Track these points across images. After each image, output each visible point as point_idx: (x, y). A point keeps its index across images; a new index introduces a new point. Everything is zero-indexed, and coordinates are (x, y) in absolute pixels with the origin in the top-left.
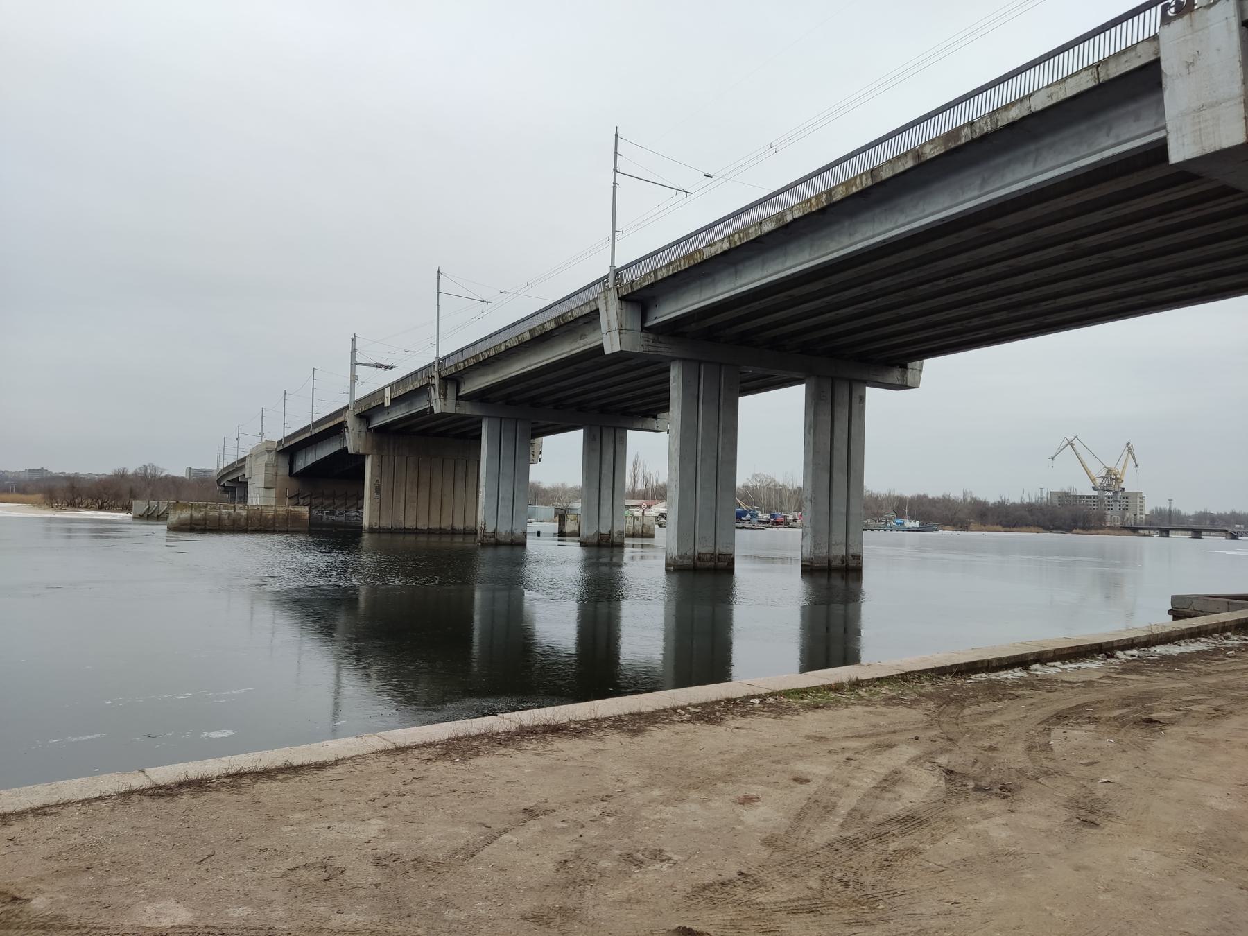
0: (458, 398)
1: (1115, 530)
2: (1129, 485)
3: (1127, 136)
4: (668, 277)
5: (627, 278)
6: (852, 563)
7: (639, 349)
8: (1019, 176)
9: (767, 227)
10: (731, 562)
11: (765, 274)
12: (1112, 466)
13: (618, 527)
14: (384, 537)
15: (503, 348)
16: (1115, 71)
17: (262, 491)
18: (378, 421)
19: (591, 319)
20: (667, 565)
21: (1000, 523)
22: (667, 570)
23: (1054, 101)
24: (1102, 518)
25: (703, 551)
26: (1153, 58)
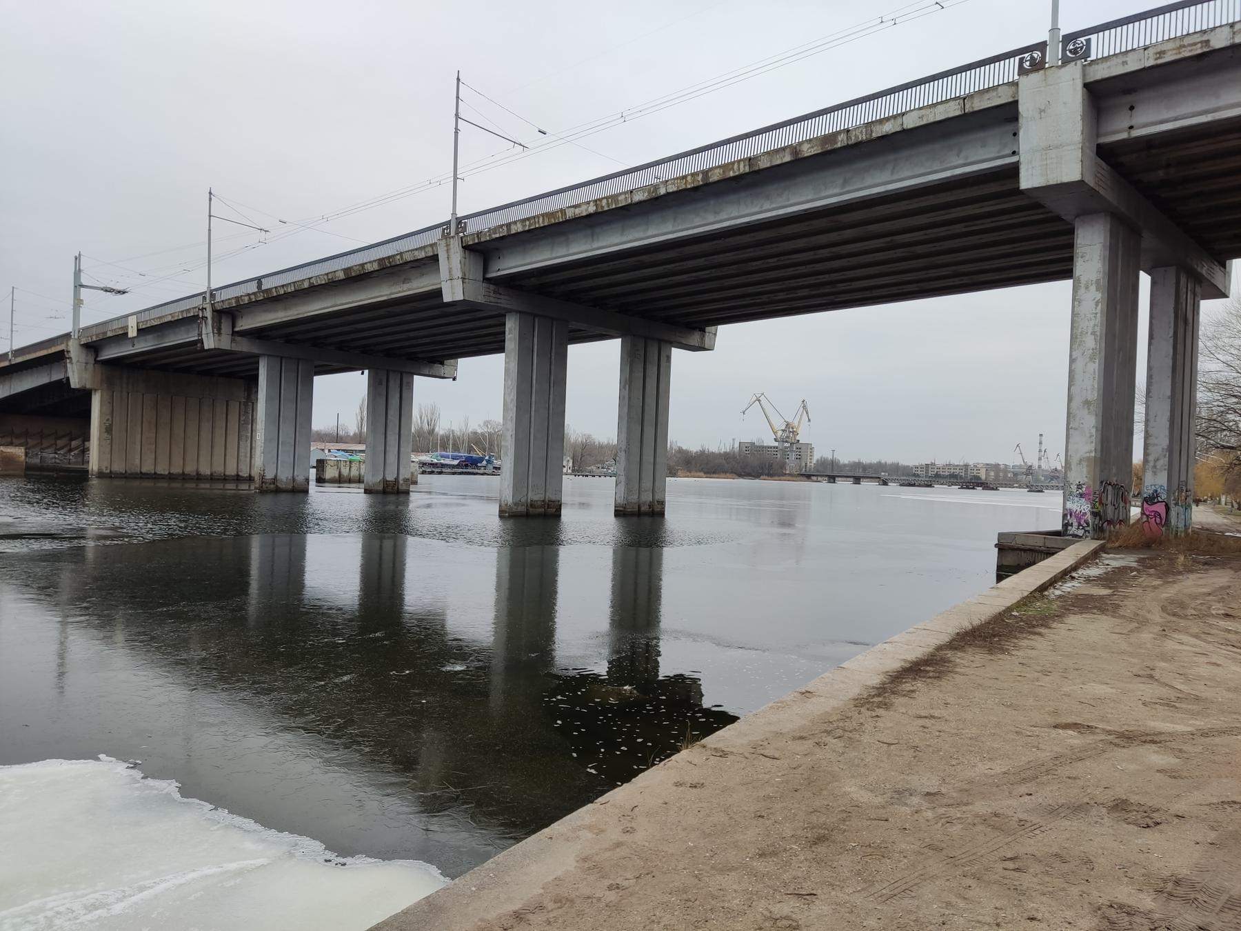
0: (234, 333)
2: (803, 438)
5: (472, 227)
6: (657, 508)
7: (481, 299)
9: (638, 197)
11: (625, 239)
13: (404, 474)
14: (117, 482)
15: (306, 285)
16: (979, 104)
18: (110, 353)
19: (430, 262)
20: (501, 511)
21: (701, 471)
22: (501, 517)
23: (924, 122)
24: (783, 466)
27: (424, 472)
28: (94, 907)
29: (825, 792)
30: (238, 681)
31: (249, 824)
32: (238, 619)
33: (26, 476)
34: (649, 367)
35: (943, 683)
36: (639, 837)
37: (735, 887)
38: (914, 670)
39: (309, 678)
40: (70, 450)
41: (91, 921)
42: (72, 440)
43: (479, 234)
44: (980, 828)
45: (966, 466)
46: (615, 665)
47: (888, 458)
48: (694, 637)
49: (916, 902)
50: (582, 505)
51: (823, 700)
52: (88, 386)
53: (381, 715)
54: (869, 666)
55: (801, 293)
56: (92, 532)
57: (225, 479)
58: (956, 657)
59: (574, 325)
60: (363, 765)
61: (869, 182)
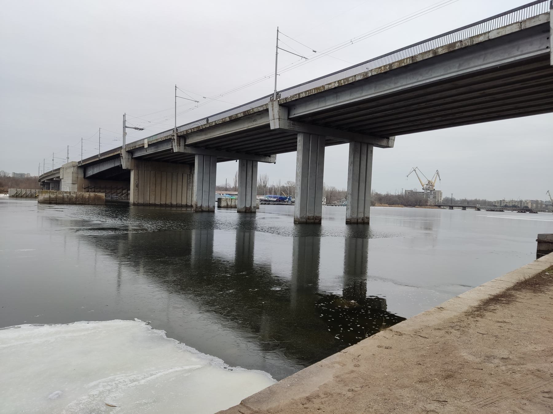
0: (185, 145)
1: (432, 206)
2: (436, 188)
3: (526, 51)
4: (306, 97)
5: (283, 96)
6: (366, 221)
7: (286, 128)
8: (476, 64)
9: (358, 78)
10: (320, 220)
11: (352, 98)
12: (430, 180)
13: (254, 204)
15: (214, 124)
17: (71, 185)
18: (138, 154)
19: (265, 112)
21: (387, 203)
22: (346, 224)
23: (500, 35)
24: (426, 201)
25: (310, 215)
26: (546, 21)
27: (262, 204)
28: (133, 381)
29: (451, 355)
30: (188, 290)
31: (194, 350)
32: (187, 265)
33: (106, 205)
34: (362, 156)
35: (510, 306)
36: (362, 369)
37: (407, 395)
38: (496, 299)
39: (216, 291)
40: (122, 194)
41: (133, 387)
42: (123, 190)
43: (286, 99)
44: (530, 376)
45: (521, 201)
46: (346, 291)
47: (481, 198)
48: (384, 280)
49: (498, 409)
50: (331, 219)
51: (449, 312)
52: (129, 168)
53: (246, 307)
54: (473, 297)
55: (437, 119)
56: (131, 228)
57: (182, 206)
58: (518, 294)
59: (328, 138)
60: (239, 328)
61: (472, 65)
